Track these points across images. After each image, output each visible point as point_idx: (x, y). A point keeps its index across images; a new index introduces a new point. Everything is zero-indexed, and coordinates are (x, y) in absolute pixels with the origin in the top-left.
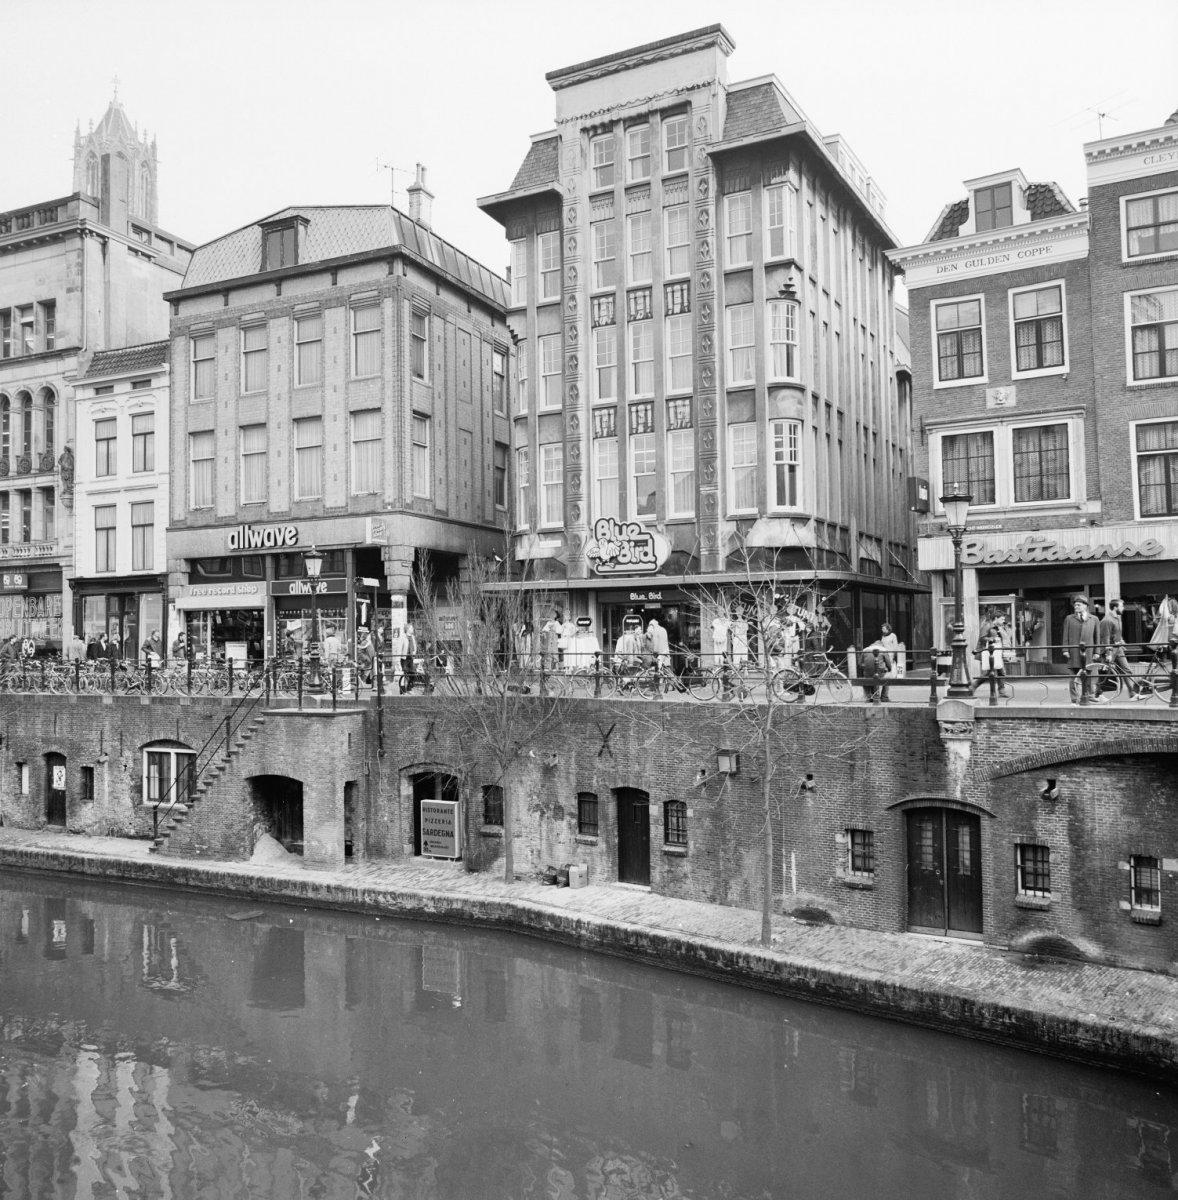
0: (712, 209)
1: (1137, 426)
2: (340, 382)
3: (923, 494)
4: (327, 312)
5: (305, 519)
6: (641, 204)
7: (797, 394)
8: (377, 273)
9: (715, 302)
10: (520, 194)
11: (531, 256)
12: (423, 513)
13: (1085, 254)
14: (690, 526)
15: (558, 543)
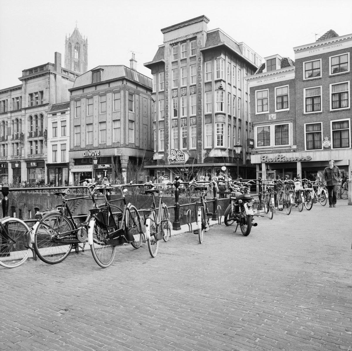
0: (202, 66)
1: (306, 125)
2: (110, 112)
3: (251, 143)
4: (107, 94)
5: (102, 149)
6: (184, 65)
7: (223, 116)
8: (119, 84)
9: (202, 91)
10: (154, 62)
11: (157, 79)
12: (132, 147)
13: (294, 78)
14: (195, 151)
15: (163, 155)
